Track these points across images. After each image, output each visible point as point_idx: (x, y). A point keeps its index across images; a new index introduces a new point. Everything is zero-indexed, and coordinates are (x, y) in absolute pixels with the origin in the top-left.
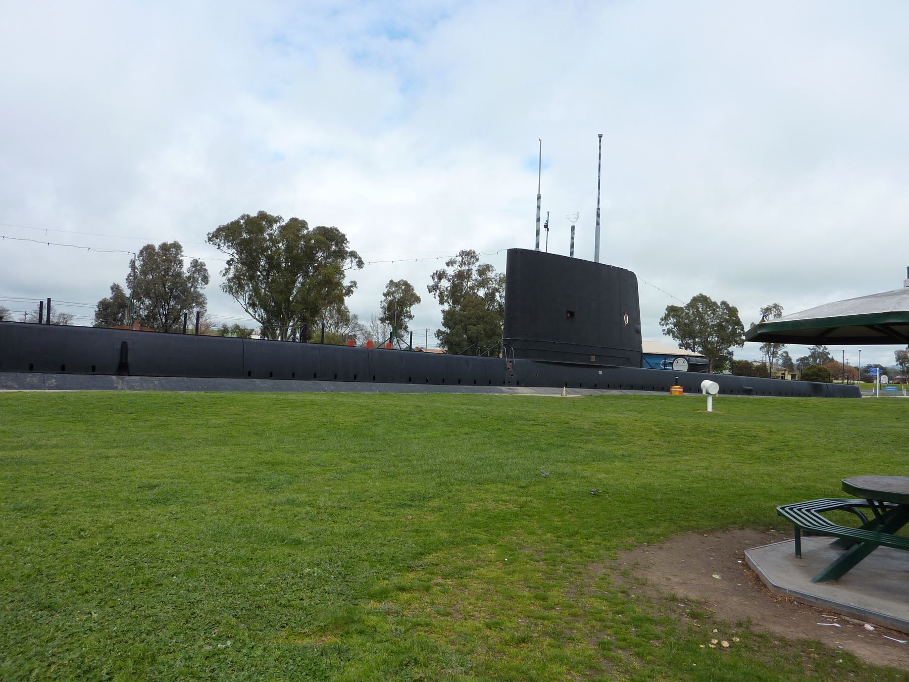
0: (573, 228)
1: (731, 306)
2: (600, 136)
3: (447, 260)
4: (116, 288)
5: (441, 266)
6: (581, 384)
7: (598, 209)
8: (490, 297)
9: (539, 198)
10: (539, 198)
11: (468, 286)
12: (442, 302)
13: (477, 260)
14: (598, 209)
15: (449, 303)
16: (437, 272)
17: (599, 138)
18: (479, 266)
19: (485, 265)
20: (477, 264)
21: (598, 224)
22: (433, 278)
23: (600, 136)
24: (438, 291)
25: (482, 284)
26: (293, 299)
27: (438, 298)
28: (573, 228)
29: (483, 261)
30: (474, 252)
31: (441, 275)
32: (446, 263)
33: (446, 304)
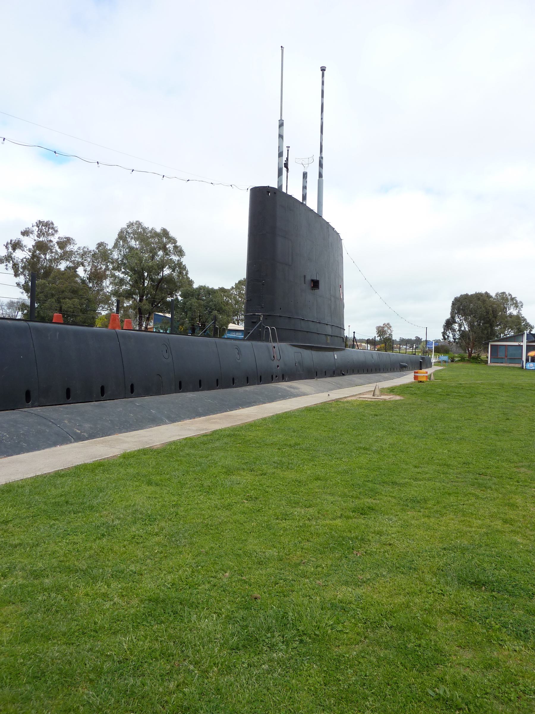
0: (305, 175)
1: (470, 294)
2: (323, 69)
3: (23, 229)
4: (422, 339)
5: (16, 236)
6: (200, 381)
7: (321, 158)
8: (72, 270)
9: (281, 125)
10: (281, 125)
11: (47, 258)
12: (16, 275)
13: (56, 231)
14: (321, 158)
15: (25, 275)
16: (11, 241)
17: (321, 72)
18: (59, 238)
19: (66, 238)
20: (57, 236)
21: (321, 176)
22: (7, 247)
23: (323, 69)
24: (11, 262)
25: (66, 255)
26: (79, 430)
27: (12, 272)
28: (305, 175)
29: (62, 233)
30: (52, 223)
31: (16, 245)
32: (22, 232)
33: (22, 277)
